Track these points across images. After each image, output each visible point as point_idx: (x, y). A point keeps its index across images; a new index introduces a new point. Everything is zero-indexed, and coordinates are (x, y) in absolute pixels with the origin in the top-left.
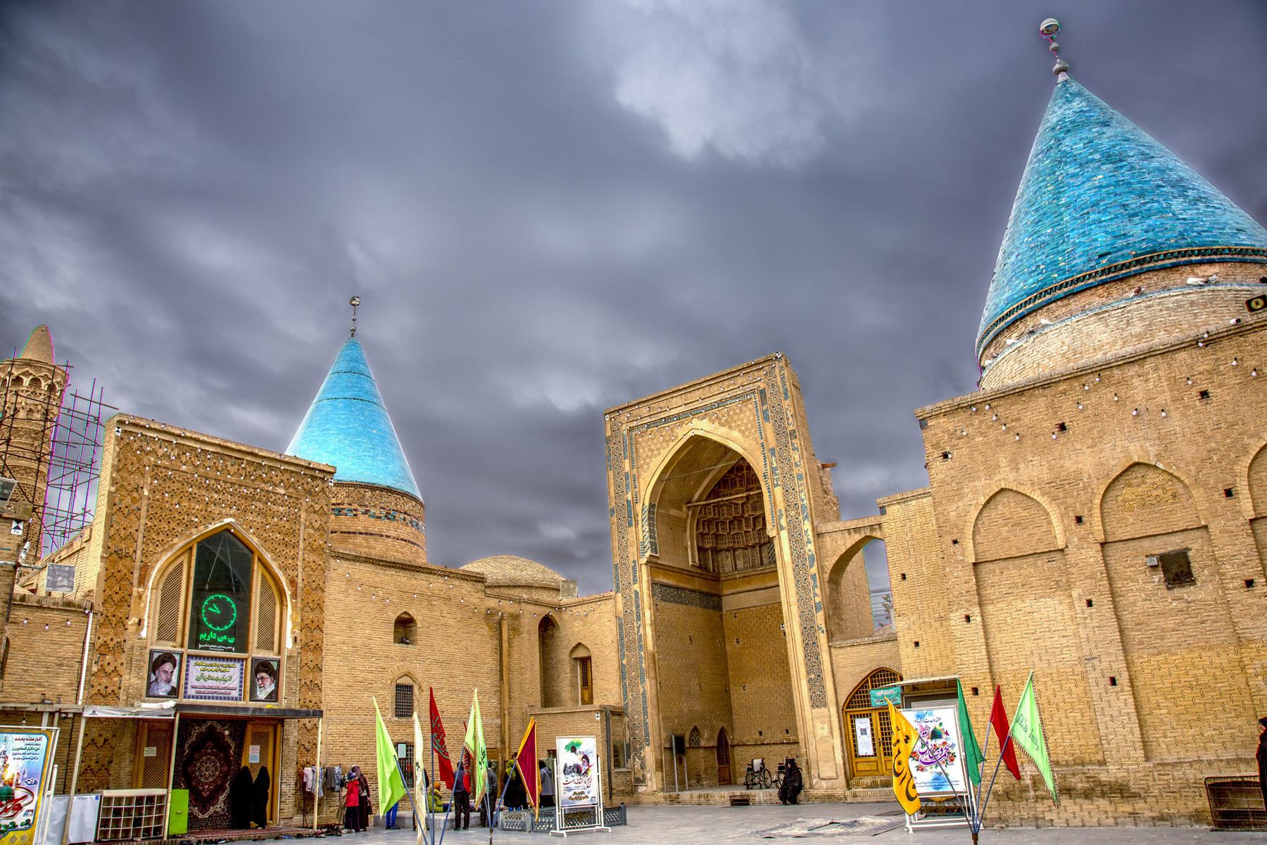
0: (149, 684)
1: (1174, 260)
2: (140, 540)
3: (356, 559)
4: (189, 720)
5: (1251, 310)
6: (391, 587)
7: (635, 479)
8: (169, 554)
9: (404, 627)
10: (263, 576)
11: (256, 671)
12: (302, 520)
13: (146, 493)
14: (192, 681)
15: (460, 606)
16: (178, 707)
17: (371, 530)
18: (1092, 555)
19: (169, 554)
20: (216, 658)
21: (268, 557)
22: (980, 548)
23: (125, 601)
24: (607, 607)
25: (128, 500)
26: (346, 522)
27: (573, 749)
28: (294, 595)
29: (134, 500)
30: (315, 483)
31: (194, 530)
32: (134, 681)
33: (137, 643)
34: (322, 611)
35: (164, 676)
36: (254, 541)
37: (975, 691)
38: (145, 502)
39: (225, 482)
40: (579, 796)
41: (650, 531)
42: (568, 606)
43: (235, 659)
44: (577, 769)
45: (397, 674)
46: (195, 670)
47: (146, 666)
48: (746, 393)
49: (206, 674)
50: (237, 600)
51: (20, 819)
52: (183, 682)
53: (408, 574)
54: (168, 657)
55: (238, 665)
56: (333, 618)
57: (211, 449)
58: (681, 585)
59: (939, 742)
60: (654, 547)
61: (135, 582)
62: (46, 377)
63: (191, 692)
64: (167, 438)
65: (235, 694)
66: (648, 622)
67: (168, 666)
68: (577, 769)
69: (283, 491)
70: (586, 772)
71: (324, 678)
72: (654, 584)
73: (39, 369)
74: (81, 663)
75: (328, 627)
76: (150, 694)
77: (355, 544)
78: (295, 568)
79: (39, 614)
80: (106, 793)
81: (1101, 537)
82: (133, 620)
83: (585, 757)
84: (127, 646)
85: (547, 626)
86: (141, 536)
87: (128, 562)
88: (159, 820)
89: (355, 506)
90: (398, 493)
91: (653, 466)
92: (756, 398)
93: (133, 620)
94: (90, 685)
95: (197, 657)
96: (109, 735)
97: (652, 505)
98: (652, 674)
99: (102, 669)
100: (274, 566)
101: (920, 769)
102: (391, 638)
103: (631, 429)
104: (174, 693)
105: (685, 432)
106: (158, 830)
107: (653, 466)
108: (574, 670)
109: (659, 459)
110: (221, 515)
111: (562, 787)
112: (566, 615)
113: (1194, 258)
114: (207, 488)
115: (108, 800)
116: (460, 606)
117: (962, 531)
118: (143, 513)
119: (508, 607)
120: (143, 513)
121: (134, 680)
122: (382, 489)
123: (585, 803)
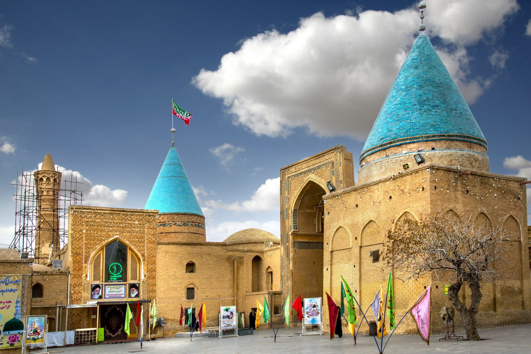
0: (92, 295)
1: (401, 143)
2: (84, 248)
3: (169, 244)
4: (104, 307)
5: (405, 169)
6: (184, 252)
7: (289, 199)
8: (95, 251)
9: (191, 267)
10: (132, 254)
12: (146, 232)
13: (84, 231)
14: (107, 293)
15: (215, 256)
16: (98, 303)
17: (177, 231)
18: (357, 250)
19: (95, 251)
20: (115, 285)
21: (133, 247)
22: (334, 246)
23: (80, 269)
24: (278, 252)
25: (78, 235)
26: (167, 229)
27: (227, 310)
28: (144, 260)
29: (80, 235)
30: (150, 218)
31: (103, 242)
32: (86, 295)
33: (86, 282)
34: (155, 264)
35: (97, 292)
36: (127, 242)
37: (356, 291)
38: (84, 235)
39: (114, 223)
40: (228, 325)
41: (294, 221)
42: (266, 251)
43: (122, 284)
44: (228, 317)
45: (187, 284)
46: (108, 289)
47: (90, 290)
48: (327, 163)
49: (112, 290)
50: (109, 272)
51: (40, 336)
53: (192, 246)
54: (98, 286)
55: (124, 286)
56: (160, 266)
57: (107, 212)
58: (311, 241)
59: (315, 309)
60: (295, 227)
61: (84, 262)
62: (52, 177)
63: (107, 296)
64: (90, 211)
65: (123, 296)
66: (291, 258)
67: (98, 289)
68: (228, 317)
69: (137, 223)
70: (232, 318)
71: (157, 288)
72: (294, 243)
73: (49, 174)
74: (68, 290)
75: (158, 270)
76: (92, 298)
77: (170, 237)
79: (52, 277)
80: (77, 330)
81: (360, 245)
82: (84, 275)
83: (232, 313)
84: (83, 284)
85: (257, 260)
86: (84, 246)
87: (80, 256)
88: (95, 337)
89: (170, 222)
90: (189, 215)
91: (295, 194)
92: (330, 165)
93: (84, 275)
94: (71, 297)
95: (108, 285)
96: (79, 312)
97: (294, 210)
98: (291, 279)
99: (75, 292)
100: (136, 250)
101: (308, 317)
102: (185, 271)
103: (289, 178)
104: (100, 297)
105: (306, 179)
106: (95, 340)
107: (295, 194)
108: (268, 276)
109: (298, 190)
111: (222, 323)
112: (265, 255)
113: (408, 141)
114: (107, 226)
115: (78, 332)
116: (215, 256)
117: (329, 240)
118: (84, 239)
119: (238, 254)
120: (84, 239)
121: (86, 294)
122: (181, 214)
123: (230, 328)
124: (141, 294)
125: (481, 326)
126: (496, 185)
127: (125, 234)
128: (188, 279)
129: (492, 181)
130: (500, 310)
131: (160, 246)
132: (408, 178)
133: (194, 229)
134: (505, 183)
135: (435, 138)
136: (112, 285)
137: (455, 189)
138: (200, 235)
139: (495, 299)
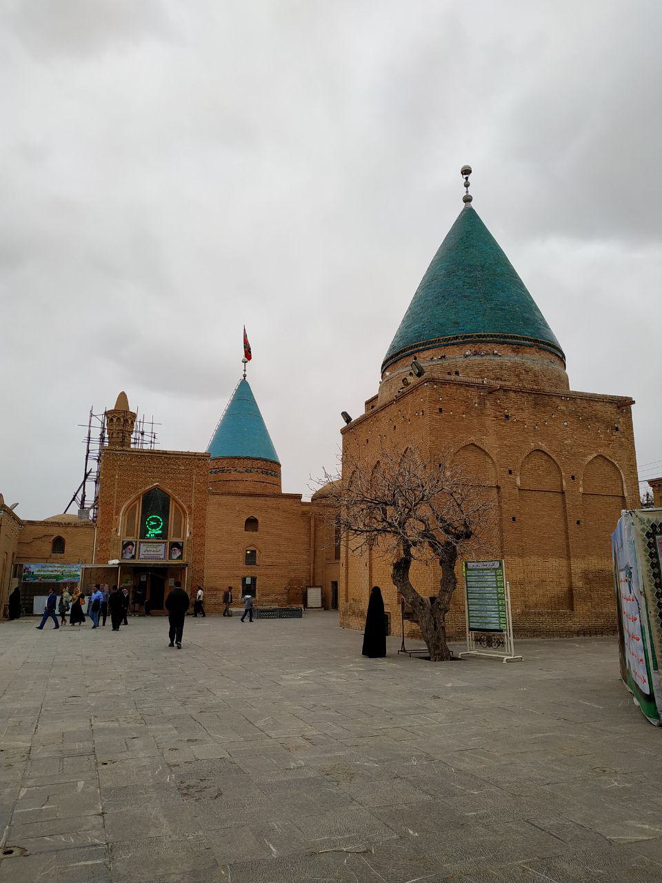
11: (171, 548)
14: (142, 552)
26: (225, 476)
28: (190, 513)
38: (117, 481)
46: (143, 547)
47: (121, 547)
52: (137, 553)
54: (130, 543)
64: (125, 453)
65: (162, 557)
67: (130, 547)
69: (183, 468)
78: (190, 501)
84: (112, 540)
89: (230, 468)
104: (133, 557)
110: (152, 483)
124: (185, 555)
125: (450, 639)
126: (567, 407)
127: (167, 481)
128: (248, 539)
129: (558, 401)
130: (581, 608)
131: (211, 497)
132: (409, 398)
133: (262, 477)
134: (586, 405)
135: (458, 341)
136: (149, 542)
137: (481, 413)
138: (268, 485)
139: (571, 590)
